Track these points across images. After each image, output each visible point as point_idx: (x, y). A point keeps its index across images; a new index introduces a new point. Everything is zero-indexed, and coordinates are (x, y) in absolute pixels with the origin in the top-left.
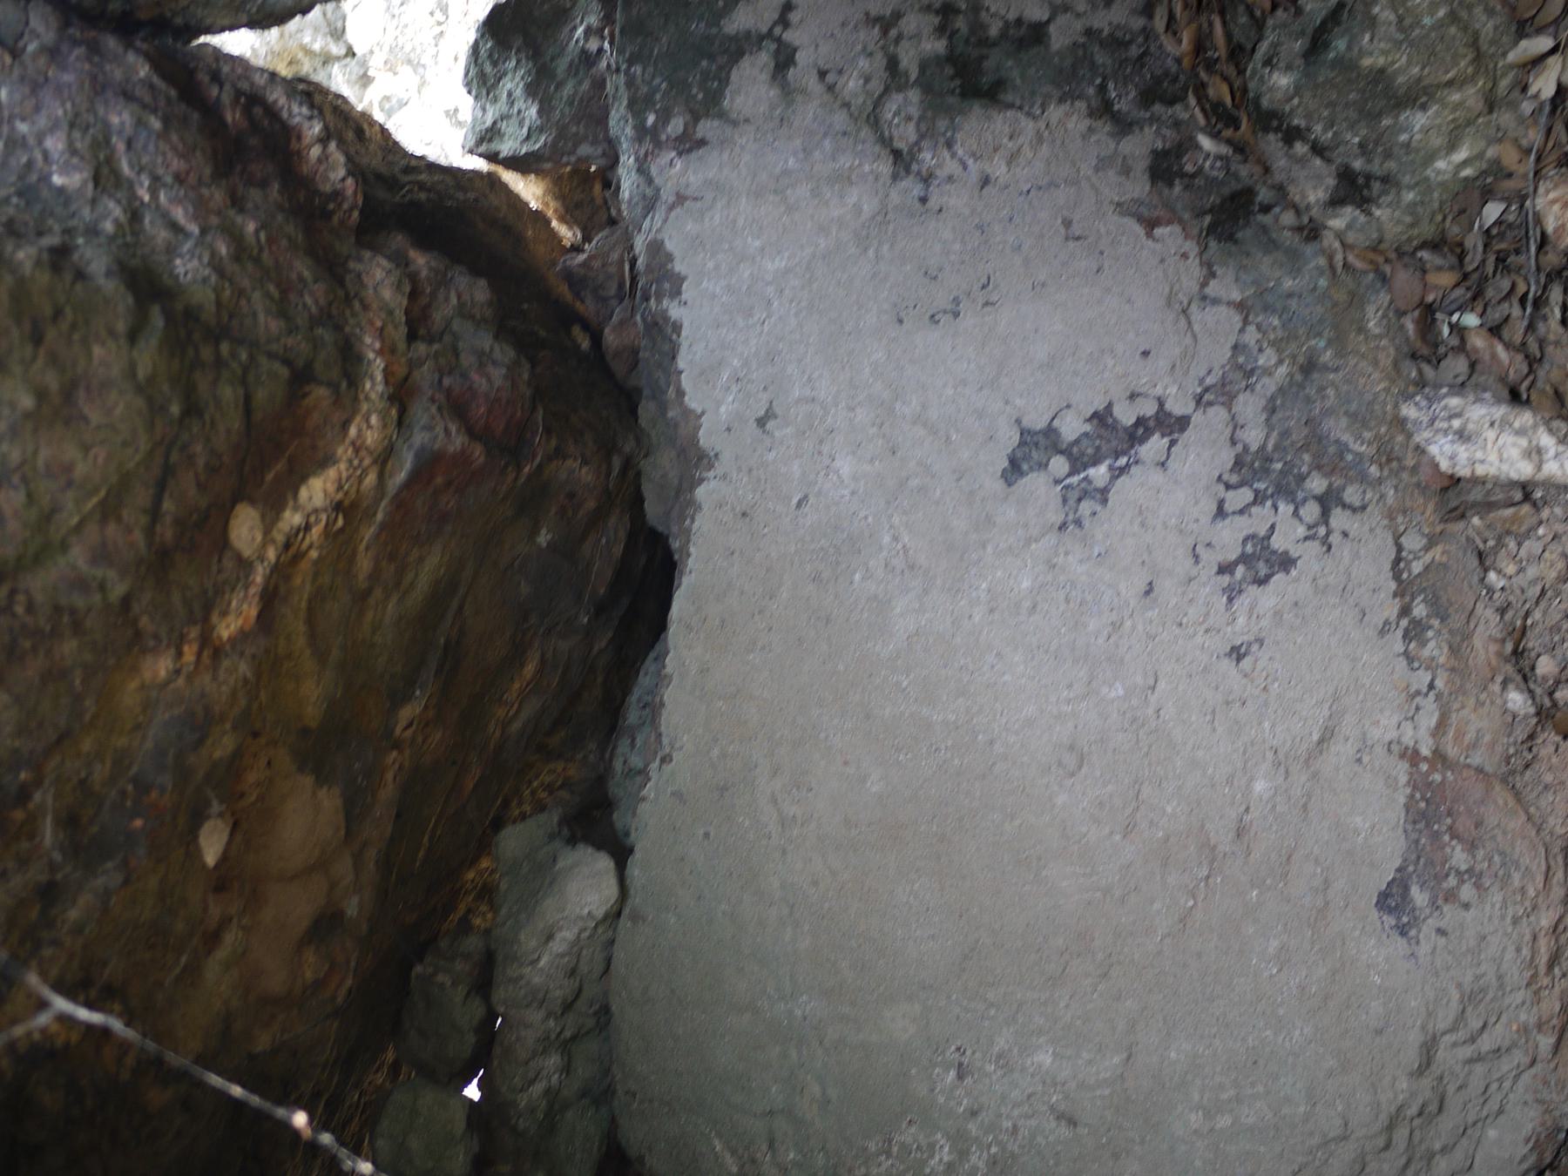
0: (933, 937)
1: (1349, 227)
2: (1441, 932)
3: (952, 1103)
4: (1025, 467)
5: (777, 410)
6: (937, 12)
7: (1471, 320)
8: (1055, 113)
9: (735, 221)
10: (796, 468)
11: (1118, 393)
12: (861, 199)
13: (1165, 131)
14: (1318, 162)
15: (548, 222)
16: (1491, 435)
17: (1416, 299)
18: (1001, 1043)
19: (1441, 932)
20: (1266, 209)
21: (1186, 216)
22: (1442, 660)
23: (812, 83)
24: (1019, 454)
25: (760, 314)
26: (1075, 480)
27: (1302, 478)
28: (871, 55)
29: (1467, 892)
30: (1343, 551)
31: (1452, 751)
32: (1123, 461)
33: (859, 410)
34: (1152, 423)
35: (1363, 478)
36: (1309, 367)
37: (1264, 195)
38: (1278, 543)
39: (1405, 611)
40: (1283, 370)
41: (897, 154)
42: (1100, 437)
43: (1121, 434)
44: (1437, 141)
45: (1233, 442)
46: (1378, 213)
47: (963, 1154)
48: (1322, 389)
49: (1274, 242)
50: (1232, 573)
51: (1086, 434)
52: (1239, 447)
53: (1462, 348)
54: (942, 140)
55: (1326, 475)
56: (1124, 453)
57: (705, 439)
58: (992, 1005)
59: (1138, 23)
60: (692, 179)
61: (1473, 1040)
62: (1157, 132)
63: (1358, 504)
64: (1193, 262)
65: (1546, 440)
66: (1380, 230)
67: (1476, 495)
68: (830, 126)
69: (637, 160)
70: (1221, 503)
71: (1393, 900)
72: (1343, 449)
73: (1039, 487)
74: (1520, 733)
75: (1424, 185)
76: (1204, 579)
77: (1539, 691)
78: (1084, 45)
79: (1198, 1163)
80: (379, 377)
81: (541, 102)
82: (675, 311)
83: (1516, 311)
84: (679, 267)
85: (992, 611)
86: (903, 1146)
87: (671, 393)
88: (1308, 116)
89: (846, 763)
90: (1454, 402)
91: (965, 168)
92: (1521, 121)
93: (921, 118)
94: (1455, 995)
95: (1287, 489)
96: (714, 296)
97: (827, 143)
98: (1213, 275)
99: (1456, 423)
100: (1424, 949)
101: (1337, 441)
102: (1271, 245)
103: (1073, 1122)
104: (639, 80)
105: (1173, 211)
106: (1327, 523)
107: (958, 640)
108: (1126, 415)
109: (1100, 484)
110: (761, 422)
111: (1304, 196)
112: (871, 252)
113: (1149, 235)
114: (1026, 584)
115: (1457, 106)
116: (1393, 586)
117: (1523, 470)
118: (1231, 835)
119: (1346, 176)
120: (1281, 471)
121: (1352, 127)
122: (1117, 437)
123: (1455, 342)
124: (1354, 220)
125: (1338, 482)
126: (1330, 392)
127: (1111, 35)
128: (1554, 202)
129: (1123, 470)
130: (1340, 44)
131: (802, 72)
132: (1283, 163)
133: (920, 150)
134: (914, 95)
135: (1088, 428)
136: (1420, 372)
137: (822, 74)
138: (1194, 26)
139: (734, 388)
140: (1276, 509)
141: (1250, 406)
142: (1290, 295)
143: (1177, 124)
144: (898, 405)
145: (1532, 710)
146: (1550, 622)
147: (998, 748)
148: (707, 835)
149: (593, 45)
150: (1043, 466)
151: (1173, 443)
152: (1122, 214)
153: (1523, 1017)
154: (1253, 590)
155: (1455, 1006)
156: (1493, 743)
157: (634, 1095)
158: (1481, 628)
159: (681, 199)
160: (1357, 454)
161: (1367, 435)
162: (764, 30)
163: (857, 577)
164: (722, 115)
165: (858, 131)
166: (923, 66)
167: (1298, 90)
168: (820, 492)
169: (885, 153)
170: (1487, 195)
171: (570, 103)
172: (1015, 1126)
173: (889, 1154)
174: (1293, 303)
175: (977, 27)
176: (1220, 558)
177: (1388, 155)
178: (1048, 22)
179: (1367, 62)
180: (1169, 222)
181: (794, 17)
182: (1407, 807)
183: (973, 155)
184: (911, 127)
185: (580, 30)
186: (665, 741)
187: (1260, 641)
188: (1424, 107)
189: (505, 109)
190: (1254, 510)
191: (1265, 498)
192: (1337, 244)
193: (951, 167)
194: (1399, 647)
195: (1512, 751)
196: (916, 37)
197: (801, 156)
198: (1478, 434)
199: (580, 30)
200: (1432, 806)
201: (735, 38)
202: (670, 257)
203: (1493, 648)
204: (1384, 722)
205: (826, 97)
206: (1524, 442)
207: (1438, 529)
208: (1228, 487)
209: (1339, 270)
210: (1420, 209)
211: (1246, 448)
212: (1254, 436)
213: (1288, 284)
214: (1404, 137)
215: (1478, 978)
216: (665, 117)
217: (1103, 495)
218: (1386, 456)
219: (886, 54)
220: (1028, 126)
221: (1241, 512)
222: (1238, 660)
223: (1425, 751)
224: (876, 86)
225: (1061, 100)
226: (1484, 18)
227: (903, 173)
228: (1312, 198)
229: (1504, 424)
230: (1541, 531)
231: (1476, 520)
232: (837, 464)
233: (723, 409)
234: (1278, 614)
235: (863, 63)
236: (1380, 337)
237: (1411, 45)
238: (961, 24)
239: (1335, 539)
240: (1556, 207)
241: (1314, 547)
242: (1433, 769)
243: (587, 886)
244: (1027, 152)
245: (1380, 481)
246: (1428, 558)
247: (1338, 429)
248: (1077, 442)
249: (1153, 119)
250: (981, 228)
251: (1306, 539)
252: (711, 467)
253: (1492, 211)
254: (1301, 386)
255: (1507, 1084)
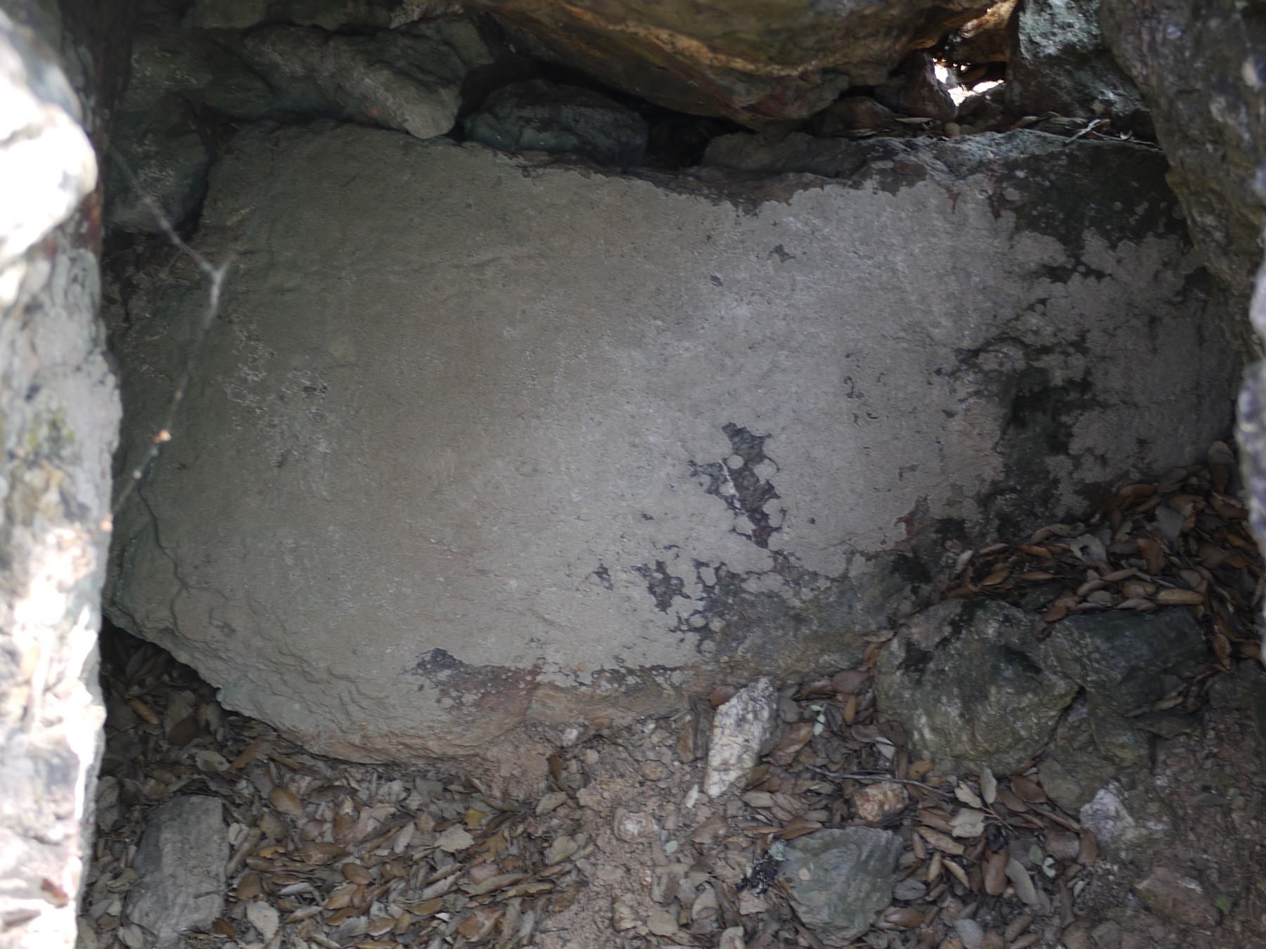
0: (402, 373)
1: (891, 653)
2: (421, 688)
3: (287, 383)
4: (736, 439)
5: (787, 263)
6: (1084, 379)
7: (818, 729)
8: (997, 461)
9: (935, 236)
10: (742, 275)
11: (787, 502)
12: (944, 328)
13: (978, 528)
14: (937, 640)
15: (977, 17)
16: (740, 740)
17: (840, 688)
18: (331, 418)
19: (421, 688)
20: (915, 591)
21: (913, 542)
22: (598, 691)
23: (1039, 292)
24: (746, 436)
25: (862, 250)
26: (726, 472)
27: (721, 615)
28: (1055, 335)
29: (447, 702)
30: (673, 638)
31: (540, 693)
32: (738, 505)
33: (783, 323)
34: (763, 524)
35: (720, 652)
36: (798, 619)
37: (926, 589)
38: (677, 601)
39: (631, 672)
40: (797, 603)
41: (975, 353)
42: (755, 490)
43: (756, 504)
44: (938, 721)
45: (748, 573)
46: (898, 673)
47: (253, 390)
48: (783, 627)
49: (891, 595)
50: (657, 571)
51: (758, 480)
52: (745, 576)
53: (802, 719)
54: (982, 388)
55: (723, 630)
56: (743, 505)
57: (769, 206)
58: (357, 412)
59: (1060, 513)
60: (970, 206)
61: (353, 701)
62: (978, 523)
63: (703, 648)
64: (879, 547)
65: (733, 775)
66: (886, 673)
67: (703, 724)
68: (1003, 307)
69: (990, 161)
70: (707, 565)
71: (441, 658)
72: (740, 641)
73: (722, 448)
74: (550, 734)
75: (913, 706)
76: (654, 552)
77: (577, 751)
78: (1047, 478)
79: (260, 545)
80: (783, 73)
81: (1057, 57)
82: (869, 184)
83: (819, 761)
84: (903, 190)
85: (633, 417)
86: (255, 349)
87: (809, 176)
88: (966, 642)
89: (524, 312)
90: (766, 714)
91: (962, 401)
92: (945, 774)
93: (1001, 373)
94: (381, 695)
95: (713, 606)
96: (879, 216)
97: (989, 304)
98: (869, 559)
99: (750, 716)
100: (409, 677)
101: (745, 637)
102: (887, 595)
103: (280, 465)
104: (1054, 163)
105: (918, 534)
106: (689, 630)
107: (612, 394)
108: (770, 507)
109: (723, 489)
110: (779, 249)
111: (916, 625)
112: (902, 334)
113: (900, 520)
114: (651, 439)
115: (959, 737)
116: (648, 666)
117: (715, 760)
118: (480, 567)
119: (925, 657)
120: (726, 603)
121: (955, 668)
122: (754, 502)
123: (807, 714)
124: (896, 658)
125: (718, 637)
126: (780, 633)
127: (1053, 495)
128: (885, 795)
129: (731, 505)
130: (1009, 673)
131: (1044, 287)
132: (942, 613)
133: (976, 373)
134: (1021, 365)
135: (762, 482)
136: (792, 686)
137: (1043, 302)
138: (1049, 556)
139: (807, 229)
140: (701, 599)
141: (774, 582)
142: (850, 607)
143: (983, 535)
144: (786, 352)
145: (565, 744)
146: (619, 763)
147: (535, 422)
148: (469, 206)
149: (1097, 107)
150: (737, 451)
151: (749, 537)
152: (918, 503)
153: (371, 728)
154: (646, 584)
155: (374, 694)
156: (547, 716)
157: (276, 145)
158: (620, 714)
159: (955, 197)
160: (736, 649)
161: (749, 655)
162: (1083, 259)
163: (659, 323)
164: (1018, 229)
165: (998, 327)
166: (1042, 371)
167: (983, 640)
168: (722, 294)
169: (978, 344)
170: (900, 748)
171: (1054, 83)
172: (274, 426)
173: (249, 338)
174: (845, 609)
175: (1069, 408)
176: (668, 563)
177: (935, 686)
178: (1068, 454)
179: (993, 690)
180: (908, 532)
181: (1091, 281)
182: (502, 668)
183: (968, 410)
184: (995, 366)
185: (1111, 96)
186: (540, 171)
187: (610, 587)
188: (962, 715)
189: (1060, 19)
190: (700, 586)
191: (709, 593)
192: (883, 639)
193: (962, 393)
194: (607, 667)
195: (540, 729)
196: (1066, 366)
197: (981, 286)
198: (741, 732)
199: (1111, 96)
200: (500, 682)
201: (1079, 238)
202: (911, 184)
203: (606, 721)
204: (558, 656)
205: (1025, 304)
206: (733, 761)
207: (685, 693)
208: (717, 569)
209: (866, 639)
210: (897, 700)
211: (744, 580)
212: (752, 585)
213: (859, 606)
214: (944, 700)
215: (393, 706)
216: (1021, 185)
217: (714, 490)
218: (733, 667)
219: (1054, 345)
220: (990, 444)
221: (699, 577)
222: (597, 573)
223: (539, 678)
224: (1029, 339)
225: (1005, 465)
226: (1016, 757)
227: (961, 357)
228: (914, 630)
229: (746, 749)
230: (676, 763)
231: (688, 718)
232: (745, 307)
233: (791, 219)
234: (629, 599)
235: (1050, 330)
236: (817, 662)
237: (1001, 716)
238: (1073, 396)
239: (679, 635)
240: (881, 797)
241: (674, 623)
242: (527, 683)
243: (425, 117)
244: (969, 443)
245: (718, 662)
246: (665, 686)
247: (754, 637)
248: (753, 475)
249: (988, 521)
250: (914, 410)
251: (680, 618)
252: (747, 212)
253: (888, 751)
254: (786, 614)
255: (328, 716)
